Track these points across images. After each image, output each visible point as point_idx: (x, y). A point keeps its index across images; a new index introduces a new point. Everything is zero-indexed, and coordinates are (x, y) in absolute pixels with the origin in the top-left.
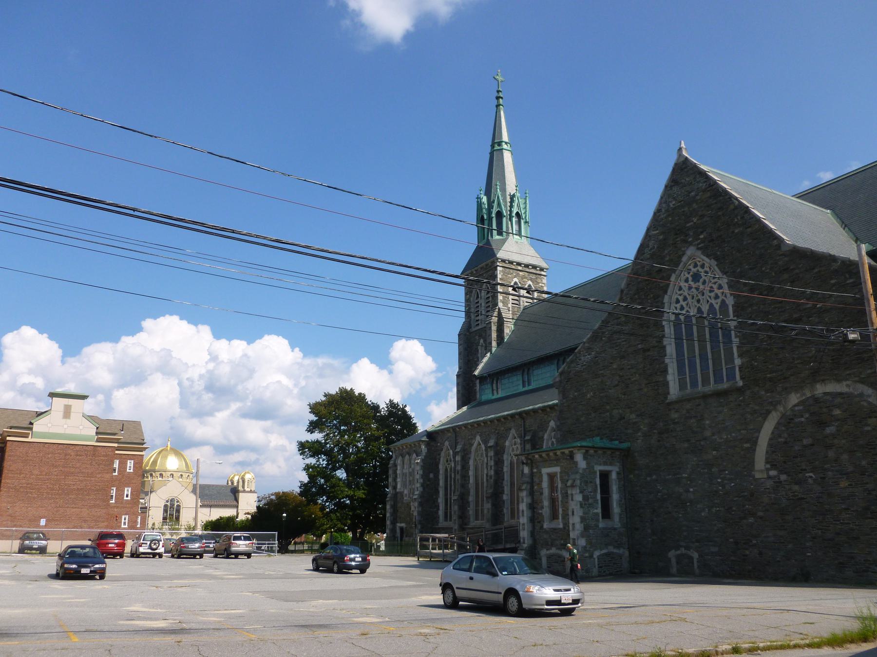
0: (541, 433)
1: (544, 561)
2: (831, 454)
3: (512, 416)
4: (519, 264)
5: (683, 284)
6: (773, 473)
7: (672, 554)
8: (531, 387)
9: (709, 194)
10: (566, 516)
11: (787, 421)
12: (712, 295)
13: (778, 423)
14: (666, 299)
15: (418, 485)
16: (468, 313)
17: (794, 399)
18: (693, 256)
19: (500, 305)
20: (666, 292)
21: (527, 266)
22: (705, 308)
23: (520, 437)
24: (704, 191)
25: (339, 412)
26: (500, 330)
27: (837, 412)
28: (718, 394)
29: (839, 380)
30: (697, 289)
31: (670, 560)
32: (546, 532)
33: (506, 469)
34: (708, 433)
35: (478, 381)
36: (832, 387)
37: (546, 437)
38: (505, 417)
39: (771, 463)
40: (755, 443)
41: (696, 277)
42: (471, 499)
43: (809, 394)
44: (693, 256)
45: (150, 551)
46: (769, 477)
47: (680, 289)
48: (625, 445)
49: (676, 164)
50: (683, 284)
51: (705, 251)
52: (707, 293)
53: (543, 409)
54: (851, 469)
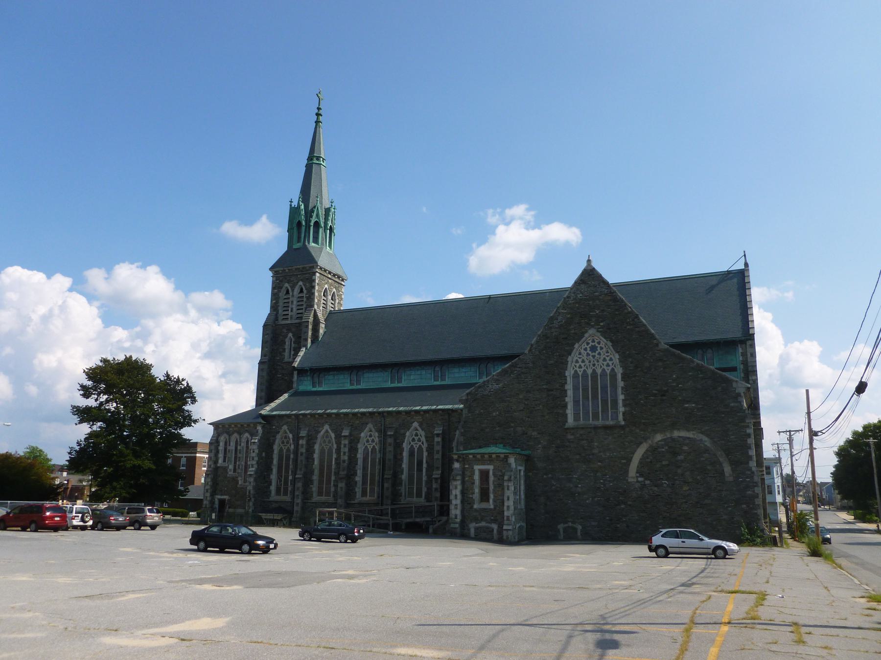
0: (402, 431)
1: (472, 531)
2: (679, 471)
3: (371, 414)
4: (330, 273)
5: (582, 351)
6: (640, 479)
7: (561, 527)
8: (359, 387)
9: (610, 298)
10: (293, 492)
11: (653, 450)
12: (605, 363)
13: (647, 450)
14: (570, 359)
15: (254, 463)
16: (274, 307)
17: (659, 437)
18: (592, 335)
19: (316, 307)
20: (570, 354)
21: (334, 275)
22: (599, 371)
23: (379, 431)
24: (606, 294)
25: (120, 378)
26: (316, 329)
27: (685, 448)
28: (606, 428)
29: (688, 431)
30: (594, 357)
31: (559, 531)
32: (476, 510)
33: (360, 456)
34: (596, 451)
35: (295, 373)
36: (683, 434)
37: (408, 434)
38: (363, 414)
39: (640, 473)
40: (629, 460)
41: (593, 349)
42: (315, 477)
43: (669, 436)
44: (592, 335)
45: (81, 524)
46: (638, 481)
47: (580, 354)
48: (527, 452)
49: (585, 270)
50: (582, 351)
51: (604, 334)
52: (601, 361)
53: (408, 413)
54: (690, 480)
